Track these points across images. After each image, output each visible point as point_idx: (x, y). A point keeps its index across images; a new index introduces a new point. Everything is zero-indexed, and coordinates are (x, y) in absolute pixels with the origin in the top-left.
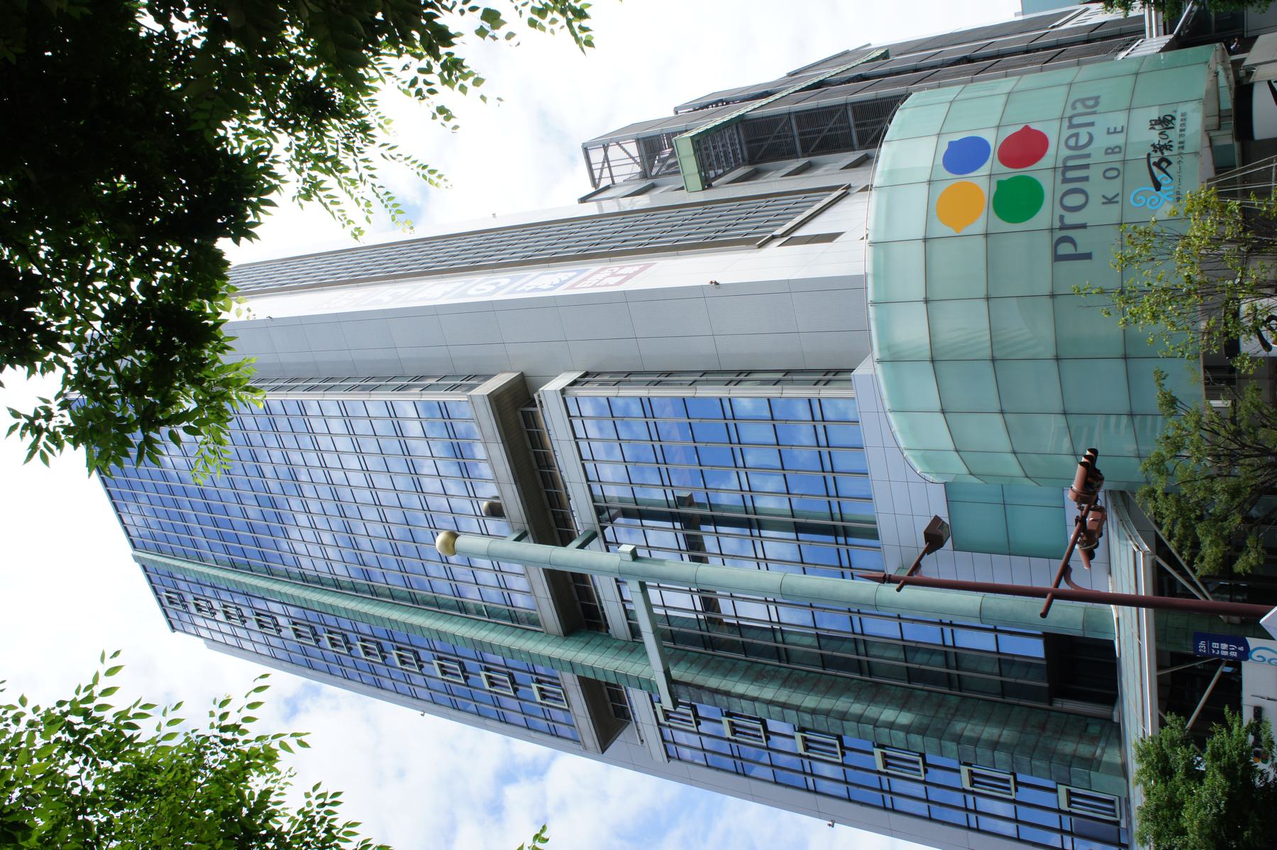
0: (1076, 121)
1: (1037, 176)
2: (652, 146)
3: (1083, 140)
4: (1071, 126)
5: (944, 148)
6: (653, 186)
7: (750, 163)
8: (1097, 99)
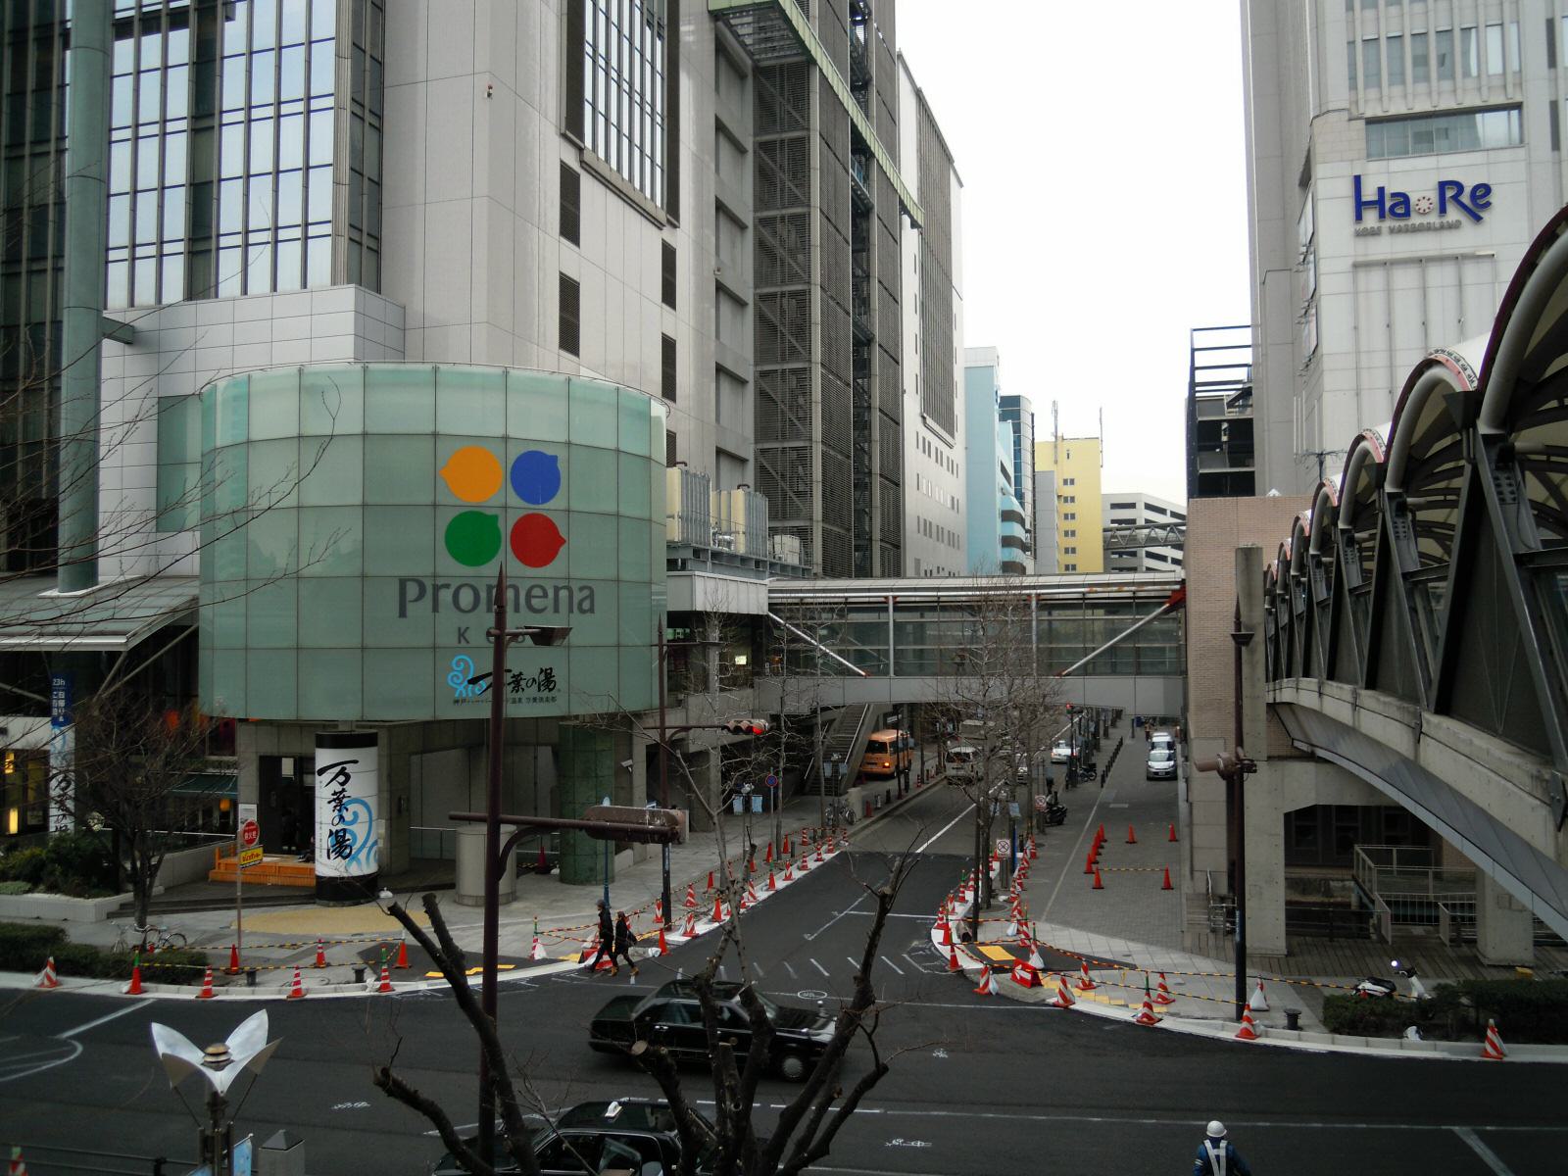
0: (563, 594)
1: (500, 557)
4: (557, 590)
5: (549, 451)
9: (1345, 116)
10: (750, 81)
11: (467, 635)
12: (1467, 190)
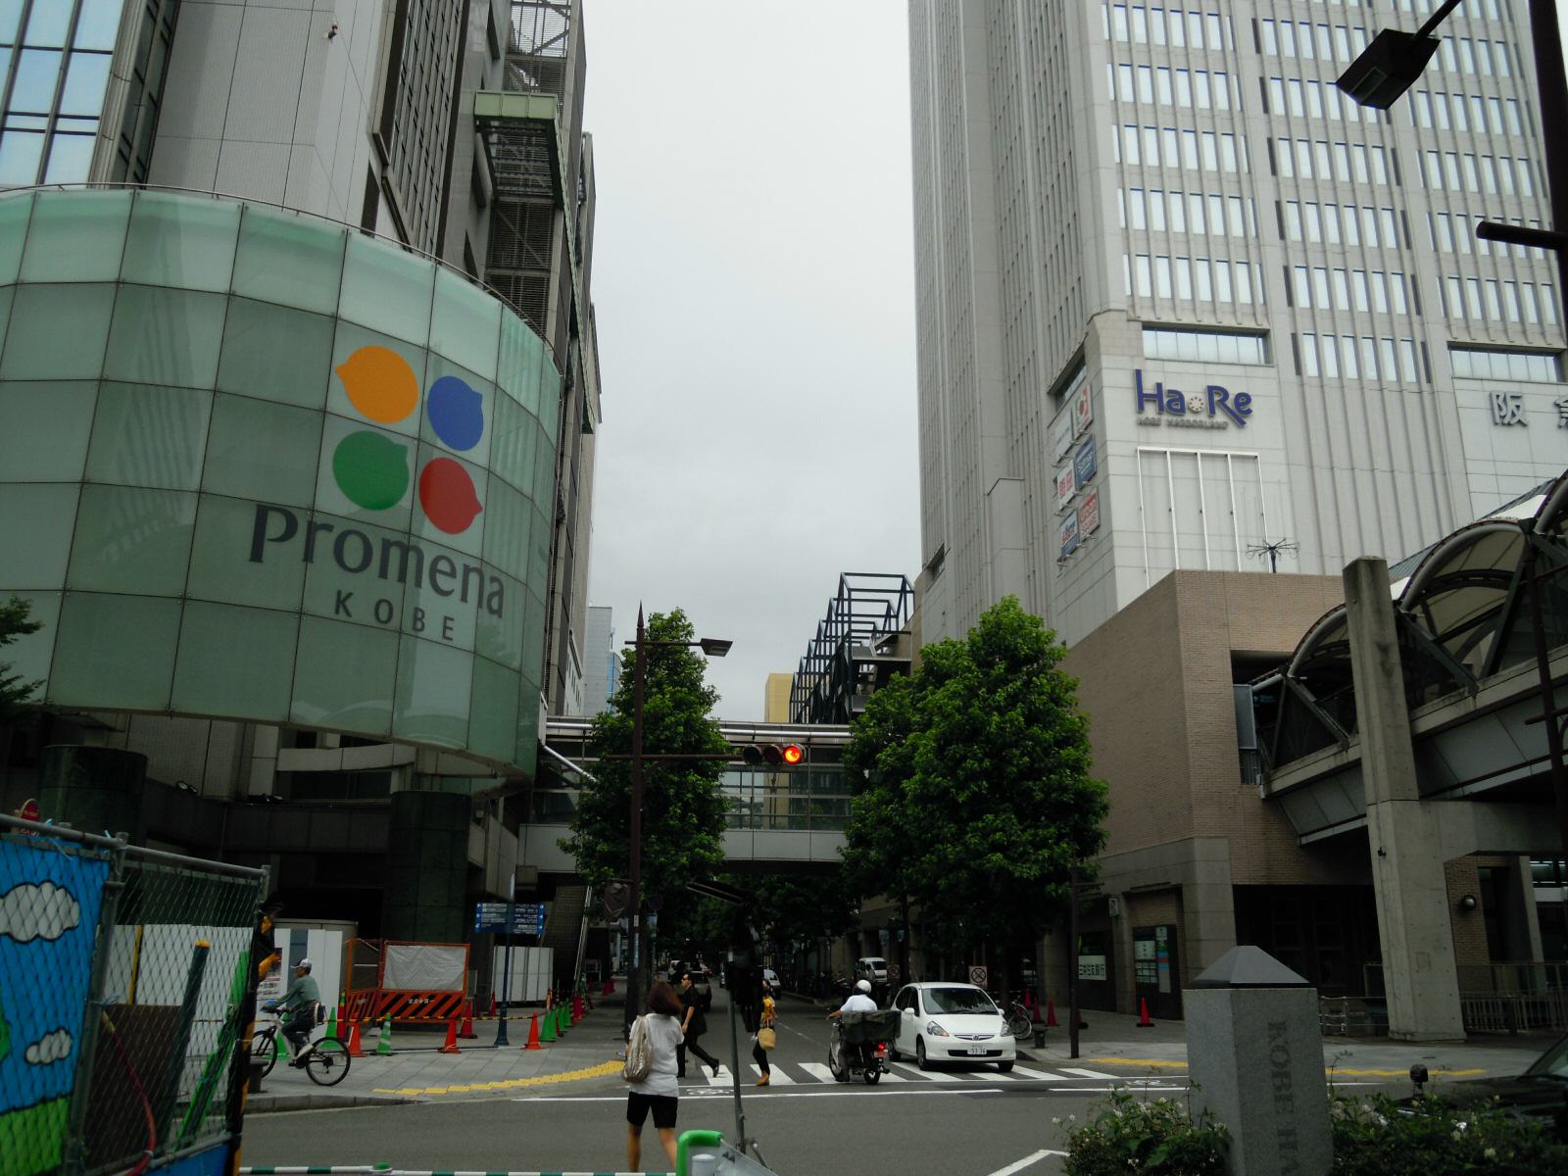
0: (474, 578)
2: (557, 74)
3: (444, 582)
4: (467, 570)
5: (476, 386)
6: (495, 57)
7: (496, 202)
8: (499, 613)
9: (1124, 317)
10: (487, 211)
11: (348, 603)
12: (1232, 397)
